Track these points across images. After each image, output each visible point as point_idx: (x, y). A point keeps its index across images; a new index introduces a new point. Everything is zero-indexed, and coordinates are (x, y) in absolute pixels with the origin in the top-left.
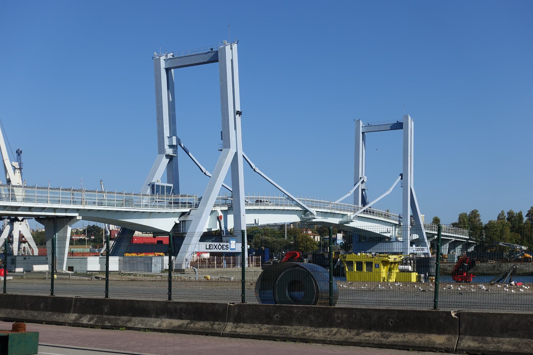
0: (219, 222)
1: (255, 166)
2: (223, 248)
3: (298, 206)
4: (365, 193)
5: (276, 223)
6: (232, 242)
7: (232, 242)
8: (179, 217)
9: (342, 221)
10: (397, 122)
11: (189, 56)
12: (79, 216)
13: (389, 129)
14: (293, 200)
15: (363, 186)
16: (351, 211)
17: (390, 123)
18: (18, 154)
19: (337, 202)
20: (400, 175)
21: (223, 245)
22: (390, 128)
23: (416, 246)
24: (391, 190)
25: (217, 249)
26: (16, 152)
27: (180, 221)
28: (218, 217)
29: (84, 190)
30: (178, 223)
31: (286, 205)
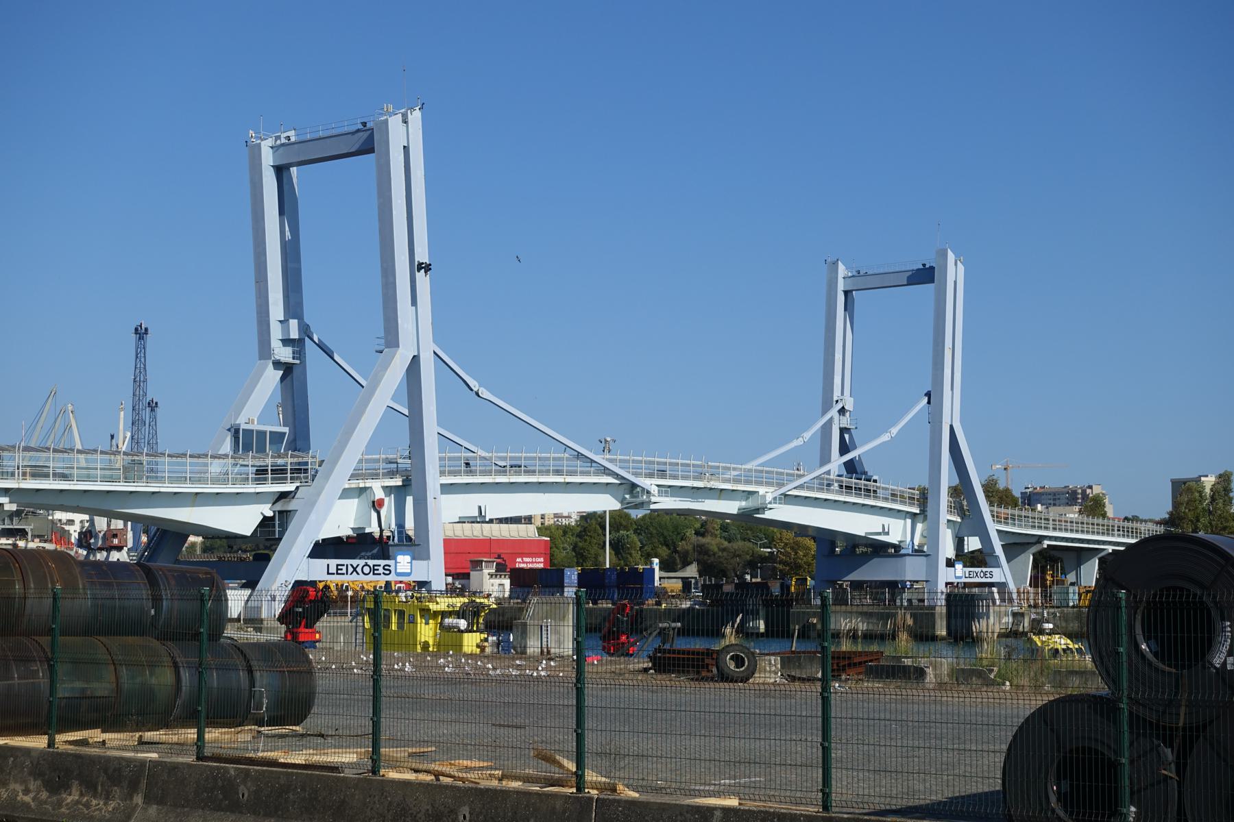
0: (376, 514)
1: (477, 385)
2: (376, 572)
3: (608, 475)
4: (851, 437)
5: (595, 510)
6: (400, 558)
7: (400, 558)
8: (274, 504)
9: (744, 507)
10: (924, 265)
11: (311, 140)
12: (10, 503)
13: (905, 283)
14: (592, 461)
15: (845, 421)
16: (768, 484)
17: (908, 269)
18: (138, 335)
19: (748, 466)
20: (926, 395)
21: (374, 566)
22: (908, 280)
23: (964, 566)
24: (895, 431)
25: (358, 574)
26: (134, 331)
27: (274, 512)
28: (373, 502)
29: (19, 447)
30: (269, 515)
31: (572, 473)
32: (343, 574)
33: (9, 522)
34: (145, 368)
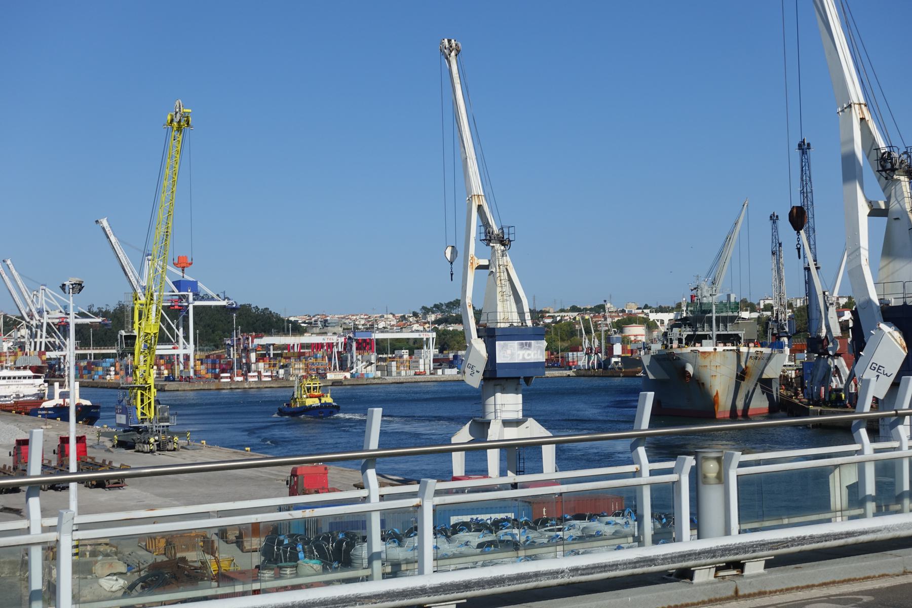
33: (708, 329)
34: (810, 180)
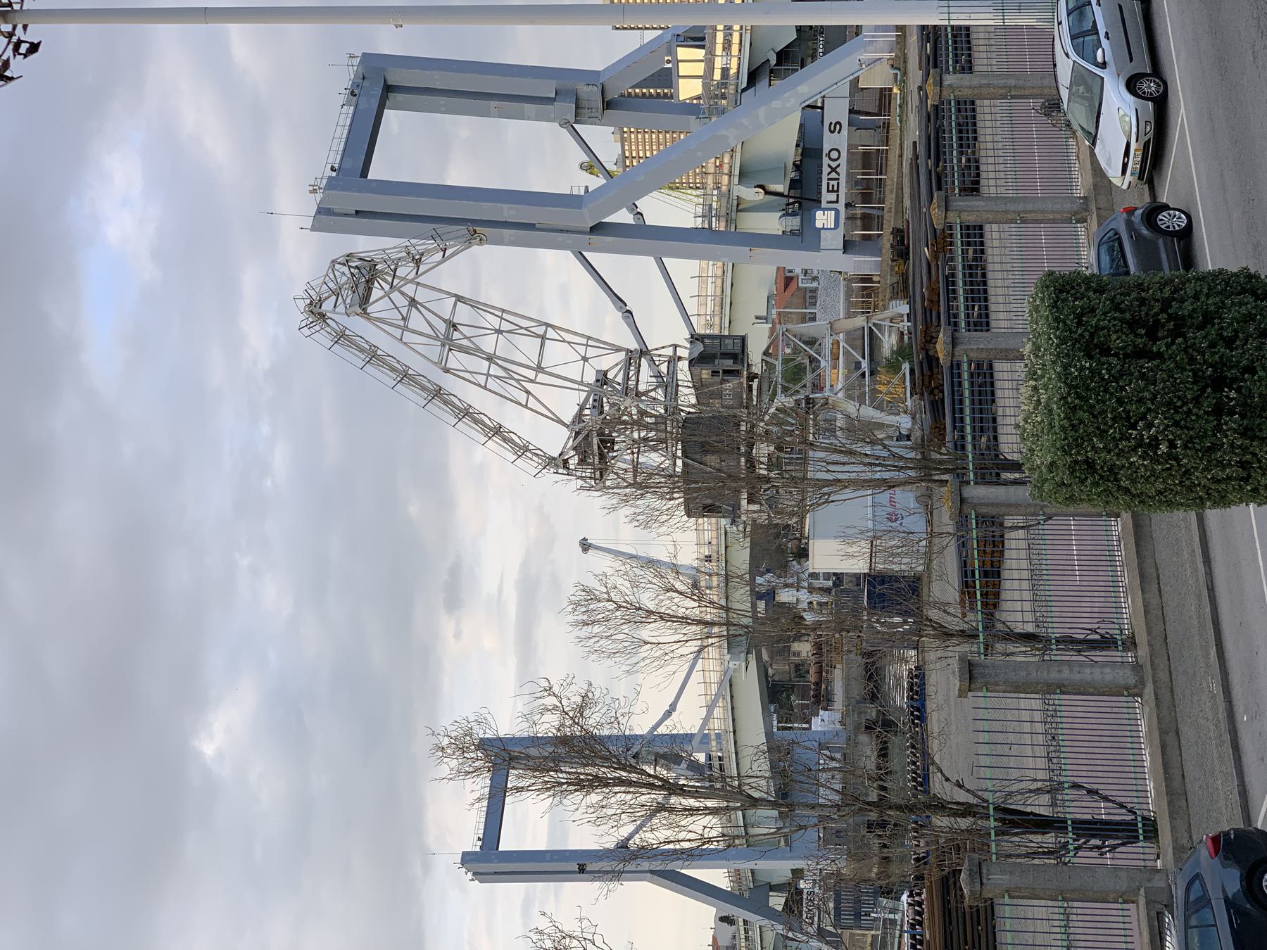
25: (839, 165)
32: (838, 183)
